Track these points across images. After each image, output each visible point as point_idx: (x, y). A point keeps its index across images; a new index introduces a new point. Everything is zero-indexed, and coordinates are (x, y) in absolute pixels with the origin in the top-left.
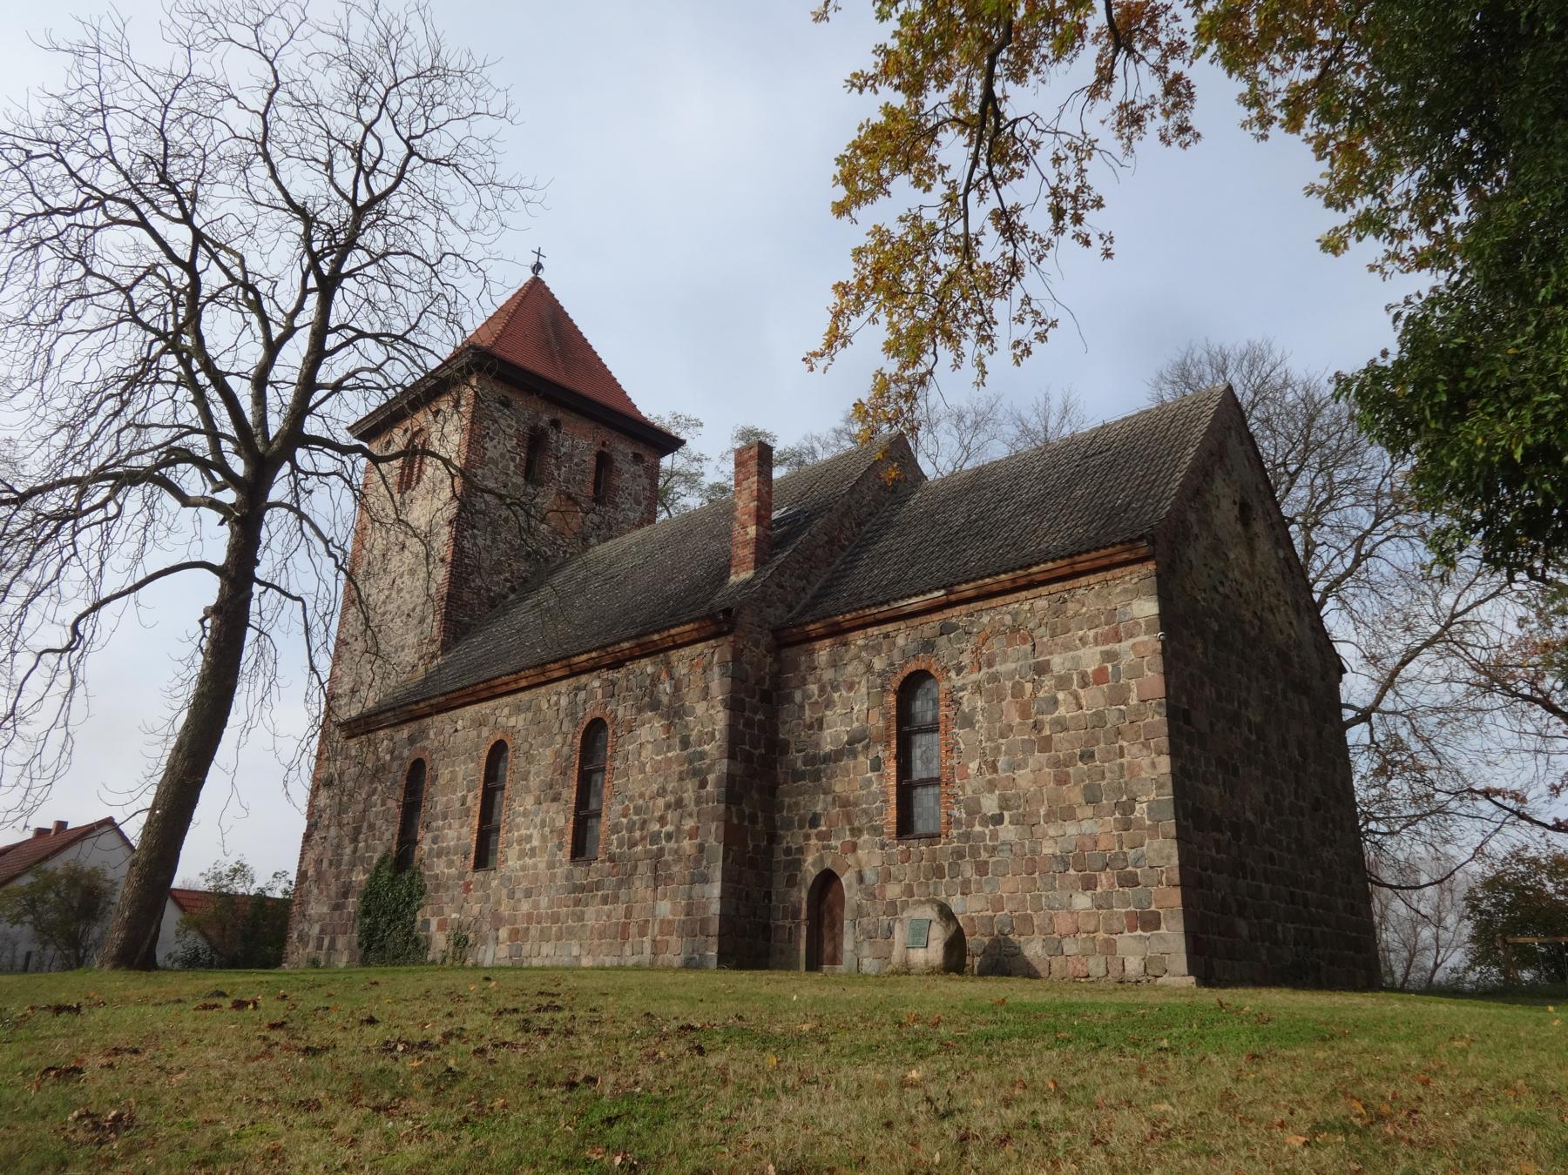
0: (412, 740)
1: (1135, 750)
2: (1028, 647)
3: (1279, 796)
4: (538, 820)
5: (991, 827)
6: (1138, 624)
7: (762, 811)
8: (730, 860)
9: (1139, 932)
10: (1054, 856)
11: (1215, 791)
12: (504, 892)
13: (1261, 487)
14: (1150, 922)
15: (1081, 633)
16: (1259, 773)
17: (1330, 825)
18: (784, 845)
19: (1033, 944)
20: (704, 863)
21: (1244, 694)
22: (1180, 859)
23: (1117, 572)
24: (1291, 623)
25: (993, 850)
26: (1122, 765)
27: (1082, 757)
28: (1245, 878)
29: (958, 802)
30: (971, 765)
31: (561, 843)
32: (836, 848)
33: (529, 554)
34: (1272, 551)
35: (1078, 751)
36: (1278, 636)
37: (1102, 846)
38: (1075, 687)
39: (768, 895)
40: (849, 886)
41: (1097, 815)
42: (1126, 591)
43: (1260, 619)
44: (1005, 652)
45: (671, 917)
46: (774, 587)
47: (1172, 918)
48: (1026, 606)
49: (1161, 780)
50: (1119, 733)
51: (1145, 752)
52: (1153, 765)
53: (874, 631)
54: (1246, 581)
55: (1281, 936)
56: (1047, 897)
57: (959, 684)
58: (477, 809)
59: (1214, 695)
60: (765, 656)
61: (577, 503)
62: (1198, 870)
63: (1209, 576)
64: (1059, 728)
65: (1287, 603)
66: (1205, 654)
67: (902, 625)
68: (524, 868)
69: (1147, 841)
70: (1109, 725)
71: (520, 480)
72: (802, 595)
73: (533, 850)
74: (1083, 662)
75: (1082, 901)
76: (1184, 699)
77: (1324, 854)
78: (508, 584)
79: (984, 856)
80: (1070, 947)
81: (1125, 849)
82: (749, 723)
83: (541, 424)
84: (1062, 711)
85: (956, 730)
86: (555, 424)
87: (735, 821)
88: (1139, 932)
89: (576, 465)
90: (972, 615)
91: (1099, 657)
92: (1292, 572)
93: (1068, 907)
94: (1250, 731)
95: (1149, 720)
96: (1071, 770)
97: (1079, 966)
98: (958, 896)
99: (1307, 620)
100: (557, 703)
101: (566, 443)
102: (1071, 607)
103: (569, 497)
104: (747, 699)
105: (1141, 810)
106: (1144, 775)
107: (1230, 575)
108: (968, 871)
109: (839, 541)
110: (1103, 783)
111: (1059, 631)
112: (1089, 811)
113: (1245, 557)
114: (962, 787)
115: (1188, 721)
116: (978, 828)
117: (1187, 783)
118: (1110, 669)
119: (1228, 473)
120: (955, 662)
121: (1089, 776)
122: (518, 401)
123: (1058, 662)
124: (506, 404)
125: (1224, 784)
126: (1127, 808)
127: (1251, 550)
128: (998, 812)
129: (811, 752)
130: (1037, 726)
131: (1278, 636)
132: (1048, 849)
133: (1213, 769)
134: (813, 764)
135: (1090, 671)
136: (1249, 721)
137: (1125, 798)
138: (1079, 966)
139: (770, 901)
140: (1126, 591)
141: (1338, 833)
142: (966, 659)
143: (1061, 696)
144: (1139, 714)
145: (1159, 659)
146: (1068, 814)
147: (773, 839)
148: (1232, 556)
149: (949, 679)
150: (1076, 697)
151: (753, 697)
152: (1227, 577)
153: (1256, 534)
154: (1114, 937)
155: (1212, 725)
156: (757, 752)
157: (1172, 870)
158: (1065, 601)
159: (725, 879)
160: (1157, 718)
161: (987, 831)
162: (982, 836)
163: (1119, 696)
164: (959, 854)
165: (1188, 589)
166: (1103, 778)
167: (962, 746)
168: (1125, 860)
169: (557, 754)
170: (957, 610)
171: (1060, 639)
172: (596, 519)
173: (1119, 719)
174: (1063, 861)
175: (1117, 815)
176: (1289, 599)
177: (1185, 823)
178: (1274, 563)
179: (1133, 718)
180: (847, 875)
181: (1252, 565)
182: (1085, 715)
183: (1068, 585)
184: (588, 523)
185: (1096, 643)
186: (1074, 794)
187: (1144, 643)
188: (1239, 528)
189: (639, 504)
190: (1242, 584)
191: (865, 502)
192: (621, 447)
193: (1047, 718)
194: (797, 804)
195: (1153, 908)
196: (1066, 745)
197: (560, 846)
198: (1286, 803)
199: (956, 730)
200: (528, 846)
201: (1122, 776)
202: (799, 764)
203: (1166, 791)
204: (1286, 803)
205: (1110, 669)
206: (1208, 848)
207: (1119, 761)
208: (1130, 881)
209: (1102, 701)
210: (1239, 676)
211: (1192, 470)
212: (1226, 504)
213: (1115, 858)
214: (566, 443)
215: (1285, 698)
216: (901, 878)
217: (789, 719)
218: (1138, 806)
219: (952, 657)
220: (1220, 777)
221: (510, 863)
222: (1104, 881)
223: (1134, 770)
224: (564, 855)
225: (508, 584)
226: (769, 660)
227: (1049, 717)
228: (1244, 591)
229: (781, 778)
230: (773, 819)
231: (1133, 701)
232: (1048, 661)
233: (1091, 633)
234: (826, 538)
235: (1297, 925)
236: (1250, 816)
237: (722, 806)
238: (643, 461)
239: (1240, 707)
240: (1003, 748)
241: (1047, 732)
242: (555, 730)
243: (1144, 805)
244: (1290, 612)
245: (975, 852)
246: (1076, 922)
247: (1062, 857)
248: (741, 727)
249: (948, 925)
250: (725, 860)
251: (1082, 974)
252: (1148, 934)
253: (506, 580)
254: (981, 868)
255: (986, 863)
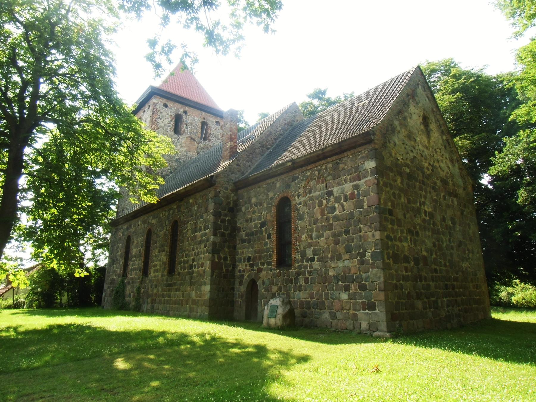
0: (127, 229)
1: (366, 229)
2: (324, 185)
3: (441, 243)
4: (159, 258)
5: (310, 263)
6: (367, 172)
7: (230, 256)
8: (214, 276)
9: (367, 311)
10: (334, 275)
11: (405, 244)
12: (150, 285)
13: (435, 109)
14: (371, 307)
15: (344, 177)
16: (430, 234)
17: (467, 252)
18: (239, 269)
19: (325, 314)
20: (205, 277)
21: (423, 200)
22: (384, 278)
23: (359, 149)
24: (449, 167)
25: (310, 273)
26: (360, 236)
27: (344, 232)
28: (421, 281)
29: (298, 252)
30: (303, 236)
31: (165, 267)
32: (255, 270)
33: (177, 160)
34: (440, 137)
35: (343, 230)
36: (442, 173)
37: (352, 272)
38: (342, 201)
39: (233, 289)
40: (260, 286)
41: (351, 258)
42: (362, 157)
43: (432, 166)
44: (316, 187)
45: (195, 298)
46: (235, 166)
47: (381, 305)
48: (324, 167)
49: (377, 242)
50: (359, 221)
51: (370, 230)
52: (373, 235)
53: (269, 181)
54: (425, 150)
55: (440, 304)
56: (331, 294)
57: (298, 202)
58: (143, 254)
59: (406, 202)
60: (231, 194)
61: (194, 140)
62: (395, 282)
63: (405, 148)
64: (336, 220)
65: (446, 158)
66: (402, 182)
67: (278, 178)
68: (155, 276)
69: (371, 270)
70: (355, 218)
71: (173, 133)
72: (249, 168)
73: (157, 269)
74: (346, 190)
75: (344, 296)
76: (389, 204)
77: (463, 265)
78: (169, 171)
79: (307, 275)
80: (339, 315)
81: (362, 273)
82: (223, 221)
83: (180, 113)
84: (337, 212)
85: (298, 222)
86: (185, 112)
87: (217, 260)
88: (367, 311)
89: (194, 126)
90: (304, 173)
91: (351, 187)
92: (449, 145)
93: (339, 298)
94: (426, 215)
95: (372, 215)
96: (340, 238)
97: (343, 325)
98: (298, 292)
99: (457, 165)
100: (165, 214)
101: (190, 119)
102: (341, 166)
103: (191, 138)
104: (222, 211)
105: (368, 256)
106: (370, 240)
107: (417, 148)
108: (302, 282)
109: (266, 146)
110: (353, 244)
111: (336, 177)
112: (347, 256)
113: (425, 139)
114: (299, 246)
115: (391, 213)
116: (305, 263)
117: (390, 243)
118: (356, 193)
119: (417, 104)
120: (297, 193)
121: (347, 241)
122: (170, 104)
123: (336, 190)
124: (166, 106)
125: (411, 241)
126: (363, 255)
127: (429, 136)
128: (312, 256)
129: (248, 231)
130: (328, 219)
131: (442, 173)
132: (331, 273)
133: (405, 235)
134: (248, 236)
135: (348, 194)
136: (425, 211)
137: (361, 251)
138: (343, 325)
139: (234, 290)
140: (362, 157)
141: (470, 255)
142: (301, 191)
143: (336, 205)
144: (368, 212)
145: (375, 187)
146: (339, 258)
147: (234, 266)
148: (418, 139)
149: (295, 200)
150: (343, 206)
151: (225, 210)
152: (415, 148)
153: (431, 130)
154: (357, 313)
155: (404, 215)
156: (227, 232)
157: (380, 283)
158: (338, 164)
159: (212, 283)
160: (375, 214)
161: (308, 265)
162: (306, 267)
163: (359, 205)
164: (298, 274)
165: (393, 154)
166: (353, 242)
167: (300, 228)
168: (362, 278)
169: (165, 234)
170: (297, 171)
171: (336, 181)
172: (202, 146)
173: (359, 215)
174: (337, 278)
175: (359, 258)
176: (448, 157)
177: (388, 261)
178: (441, 141)
179: (365, 214)
180: (259, 281)
181: (429, 142)
182: (346, 214)
183: (339, 156)
184: (199, 147)
185: (351, 182)
186: (341, 249)
187: (370, 180)
188: (422, 127)
189: (219, 139)
190: (423, 151)
191: (278, 130)
192: (211, 119)
193: (331, 215)
194: (243, 252)
195: (373, 300)
196: (338, 227)
197: (165, 269)
198: (444, 245)
199: (298, 222)
200: (156, 268)
201: (360, 241)
202: (244, 236)
203: (378, 247)
204: (444, 245)
205: (356, 193)
206: (401, 271)
207: (359, 234)
208: (363, 287)
209: (352, 207)
210: (420, 192)
211: (397, 102)
212: (415, 117)
213: (357, 277)
214: (190, 119)
215: (444, 198)
216: (278, 283)
217: (240, 218)
218: (367, 254)
219: (296, 191)
220: (409, 238)
221: (151, 274)
222: (353, 288)
223: (365, 238)
224: (165, 273)
225: (169, 171)
226: (232, 195)
227: (332, 215)
228: (424, 154)
229: (238, 242)
230: (235, 258)
231: (365, 207)
232: (332, 190)
233: (348, 177)
234: (260, 145)
235: (448, 298)
236: (425, 253)
237: (211, 255)
238: (219, 124)
239: (420, 205)
240: (315, 229)
241: (331, 222)
242: (164, 225)
243: (370, 254)
244: (448, 162)
245: (304, 274)
246: (342, 305)
247: (336, 276)
248: (219, 223)
249: (285, 308)
250: (212, 276)
251: (344, 328)
252: (370, 312)
253: (169, 169)
254: (306, 280)
255: (308, 278)
